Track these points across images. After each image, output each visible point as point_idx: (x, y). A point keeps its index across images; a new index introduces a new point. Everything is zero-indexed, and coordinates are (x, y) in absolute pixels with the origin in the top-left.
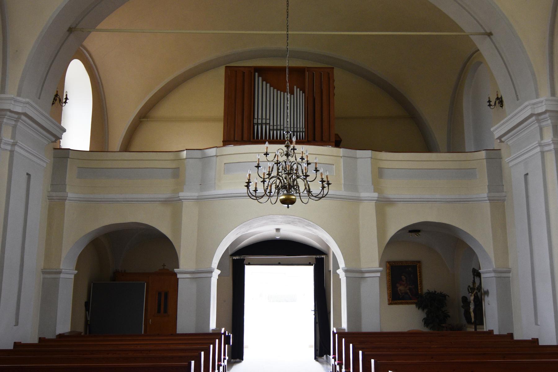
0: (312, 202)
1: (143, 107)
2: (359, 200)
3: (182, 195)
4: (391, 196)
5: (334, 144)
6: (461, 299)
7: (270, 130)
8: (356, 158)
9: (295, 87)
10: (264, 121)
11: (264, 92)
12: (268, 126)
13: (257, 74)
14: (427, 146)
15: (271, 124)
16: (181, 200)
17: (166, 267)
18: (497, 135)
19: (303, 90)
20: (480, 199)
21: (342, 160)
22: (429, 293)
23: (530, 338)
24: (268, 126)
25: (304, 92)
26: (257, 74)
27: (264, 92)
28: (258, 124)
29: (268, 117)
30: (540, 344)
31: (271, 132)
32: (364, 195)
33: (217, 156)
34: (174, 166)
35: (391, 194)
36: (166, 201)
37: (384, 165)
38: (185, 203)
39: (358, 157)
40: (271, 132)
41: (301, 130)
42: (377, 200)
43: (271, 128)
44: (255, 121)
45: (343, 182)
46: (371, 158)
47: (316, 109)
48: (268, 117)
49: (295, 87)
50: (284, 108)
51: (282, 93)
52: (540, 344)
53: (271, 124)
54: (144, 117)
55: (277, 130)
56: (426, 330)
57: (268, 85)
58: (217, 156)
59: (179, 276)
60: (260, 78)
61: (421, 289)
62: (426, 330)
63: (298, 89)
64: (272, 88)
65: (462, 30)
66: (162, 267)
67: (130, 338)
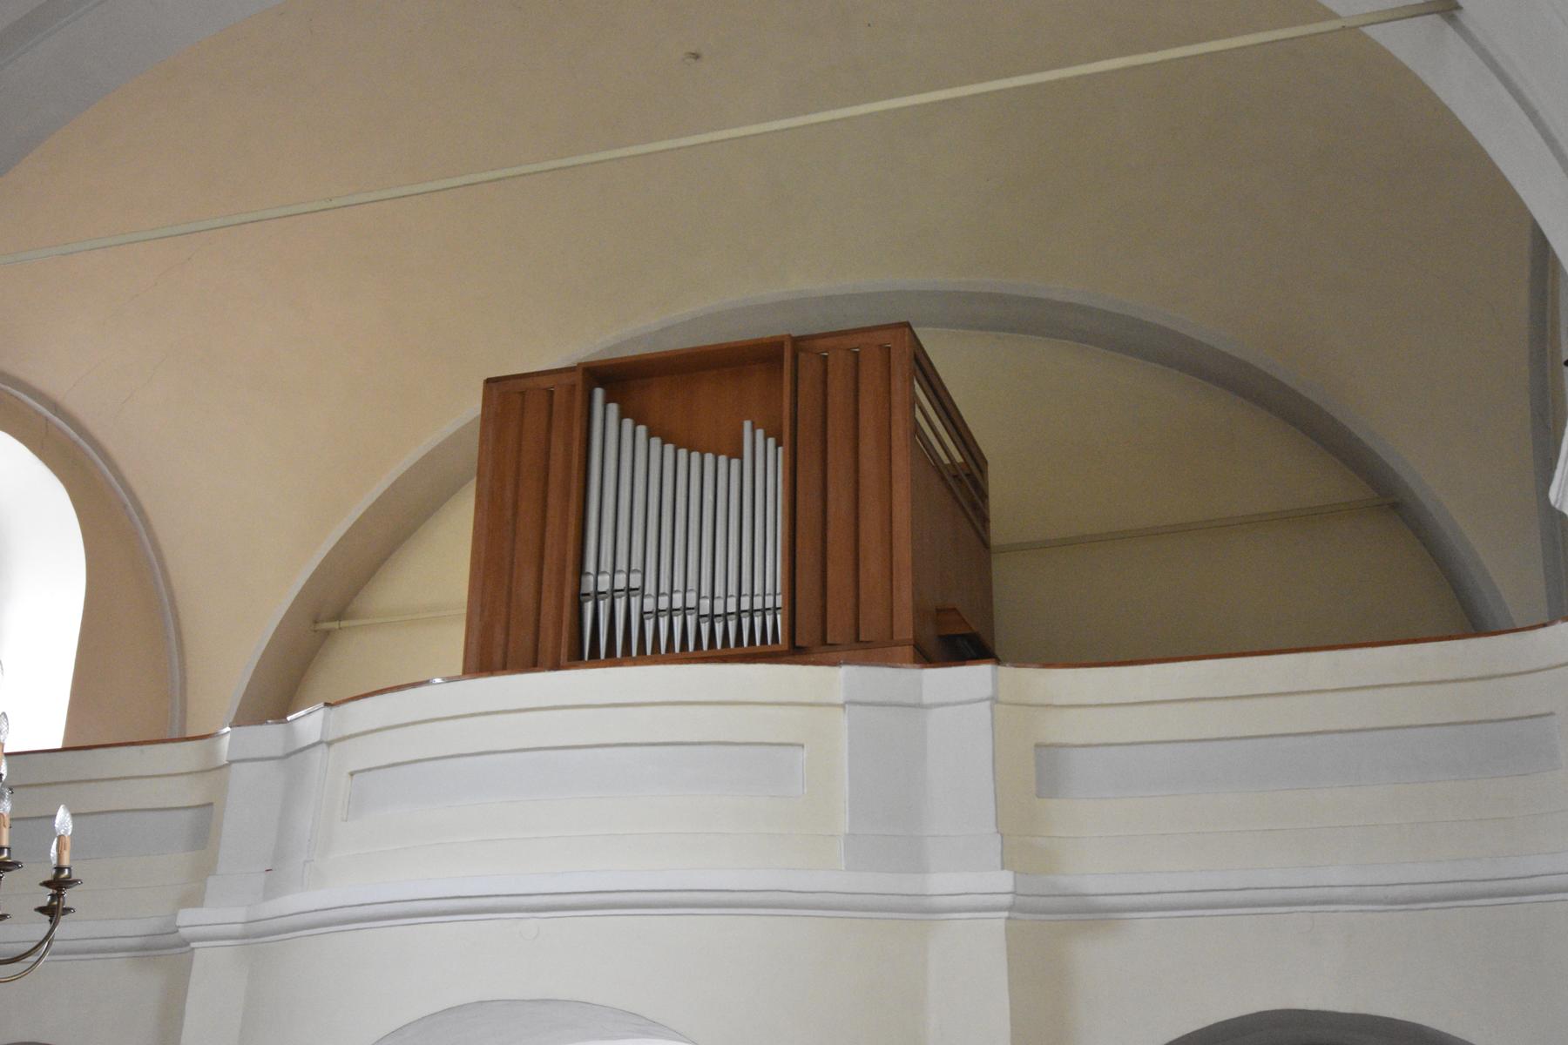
1: (315, 574)
2: (922, 911)
3: (189, 919)
4: (1091, 885)
5: (908, 650)
7: (642, 614)
8: (919, 706)
9: (747, 425)
10: (621, 582)
11: (627, 461)
12: (635, 602)
13: (599, 393)
14: (1470, 618)
15: (650, 588)
16: (185, 943)
19: (773, 432)
20: (276, 924)
21: (842, 720)
26: (599, 393)
27: (627, 461)
29: (636, 563)
31: (649, 625)
32: (942, 883)
33: (329, 744)
34: (192, 793)
35: (1094, 873)
36: (144, 948)
37: (1057, 729)
38: (203, 955)
39: (927, 699)
40: (649, 625)
41: (769, 604)
42: (1010, 909)
46: (994, 700)
47: (832, 509)
48: (636, 563)
49: (747, 425)
50: (693, 517)
53: (650, 588)
54: (340, 615)
57: (642, 429)
58: (329, 744)
63: (760, 433)
64: (656, 442)
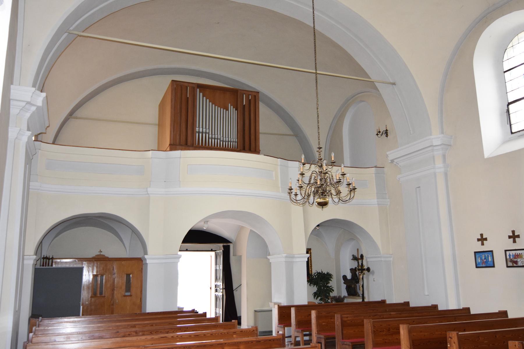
0: (341, 205)
6: (342, 278)
12: (207, 135)
13: (198, 90)
15: (210, 133)
17: (102, 253)
18: (391, 157)
22: (319, 274)
23: (430, 305)
24: (207, 135)
25: (236, 109)
28: (199, 132)
30: (439, 309)
31: (210, 140)
40: (210, 140)
43: (210, 136)
44: (197, 129)
45: (280, 186)
50: (221, 121)
51: (216, 107)
52: (439, 309)
53: (210, 133)
55: (215, 139)
56: (317, 301)
57: (208, 100)
59: (148, 261)
60: (201, 94)
61: (311, 272)
62: (317, 301)
65: (370, 78)
66: (99, 253)
67: (141, 318)
